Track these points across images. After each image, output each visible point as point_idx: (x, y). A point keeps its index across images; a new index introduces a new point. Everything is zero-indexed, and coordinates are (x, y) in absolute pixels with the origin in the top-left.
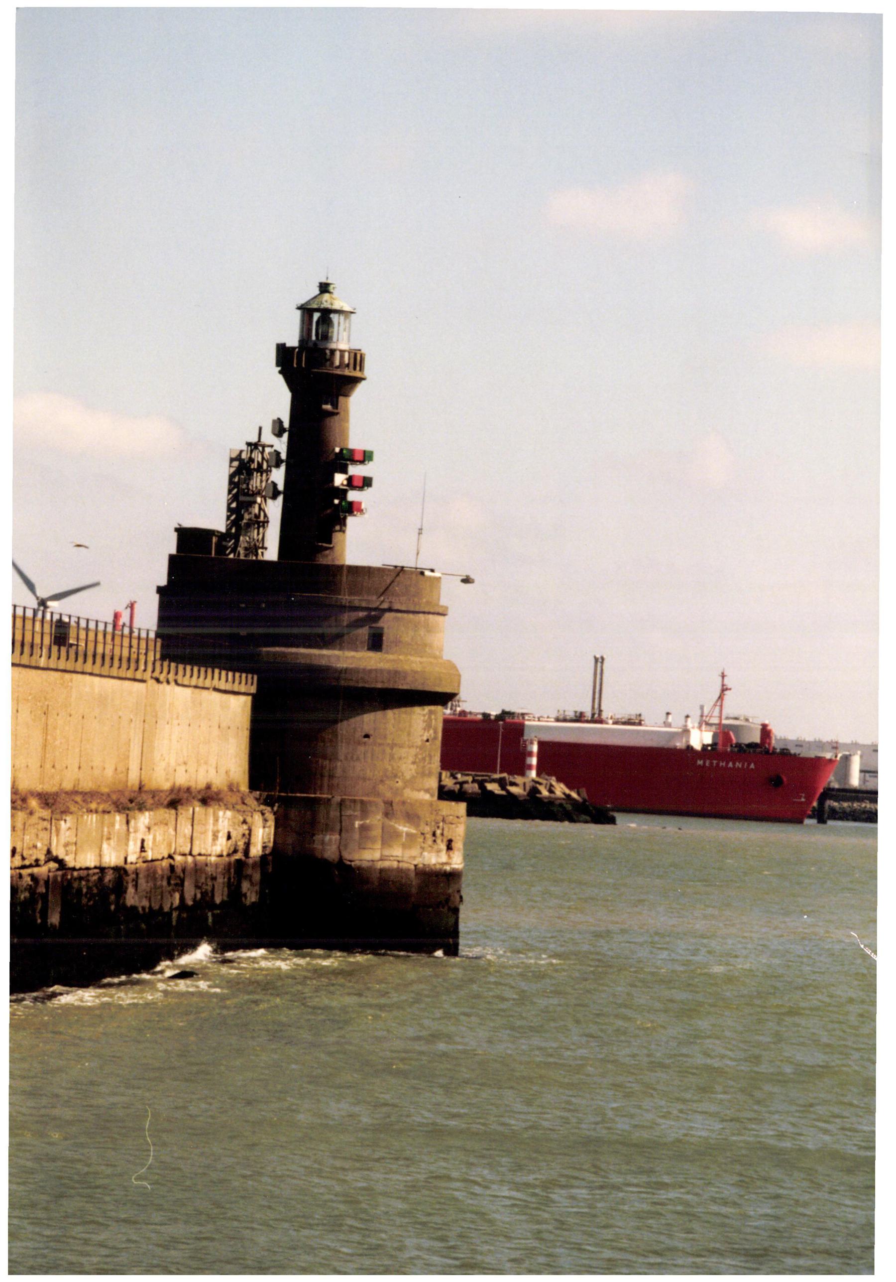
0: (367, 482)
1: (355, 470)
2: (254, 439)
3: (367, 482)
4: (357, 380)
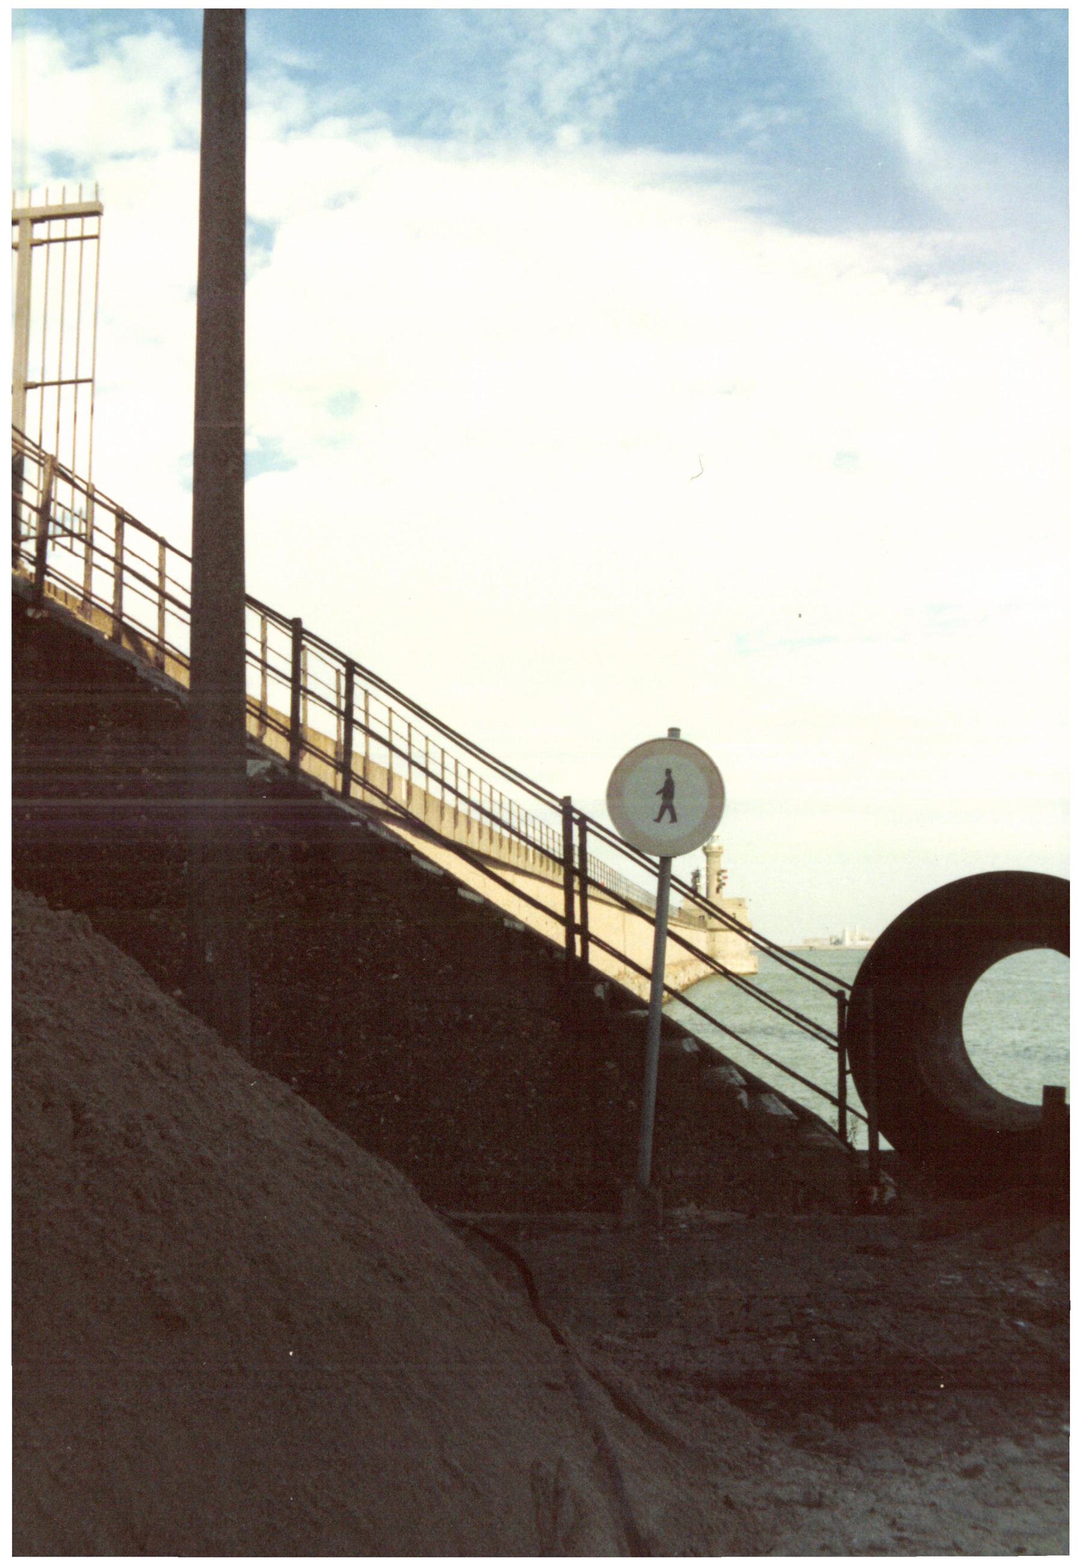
0: (725, 878)
1: (723, 874)
3: (725, 878)
4: (722, 852)
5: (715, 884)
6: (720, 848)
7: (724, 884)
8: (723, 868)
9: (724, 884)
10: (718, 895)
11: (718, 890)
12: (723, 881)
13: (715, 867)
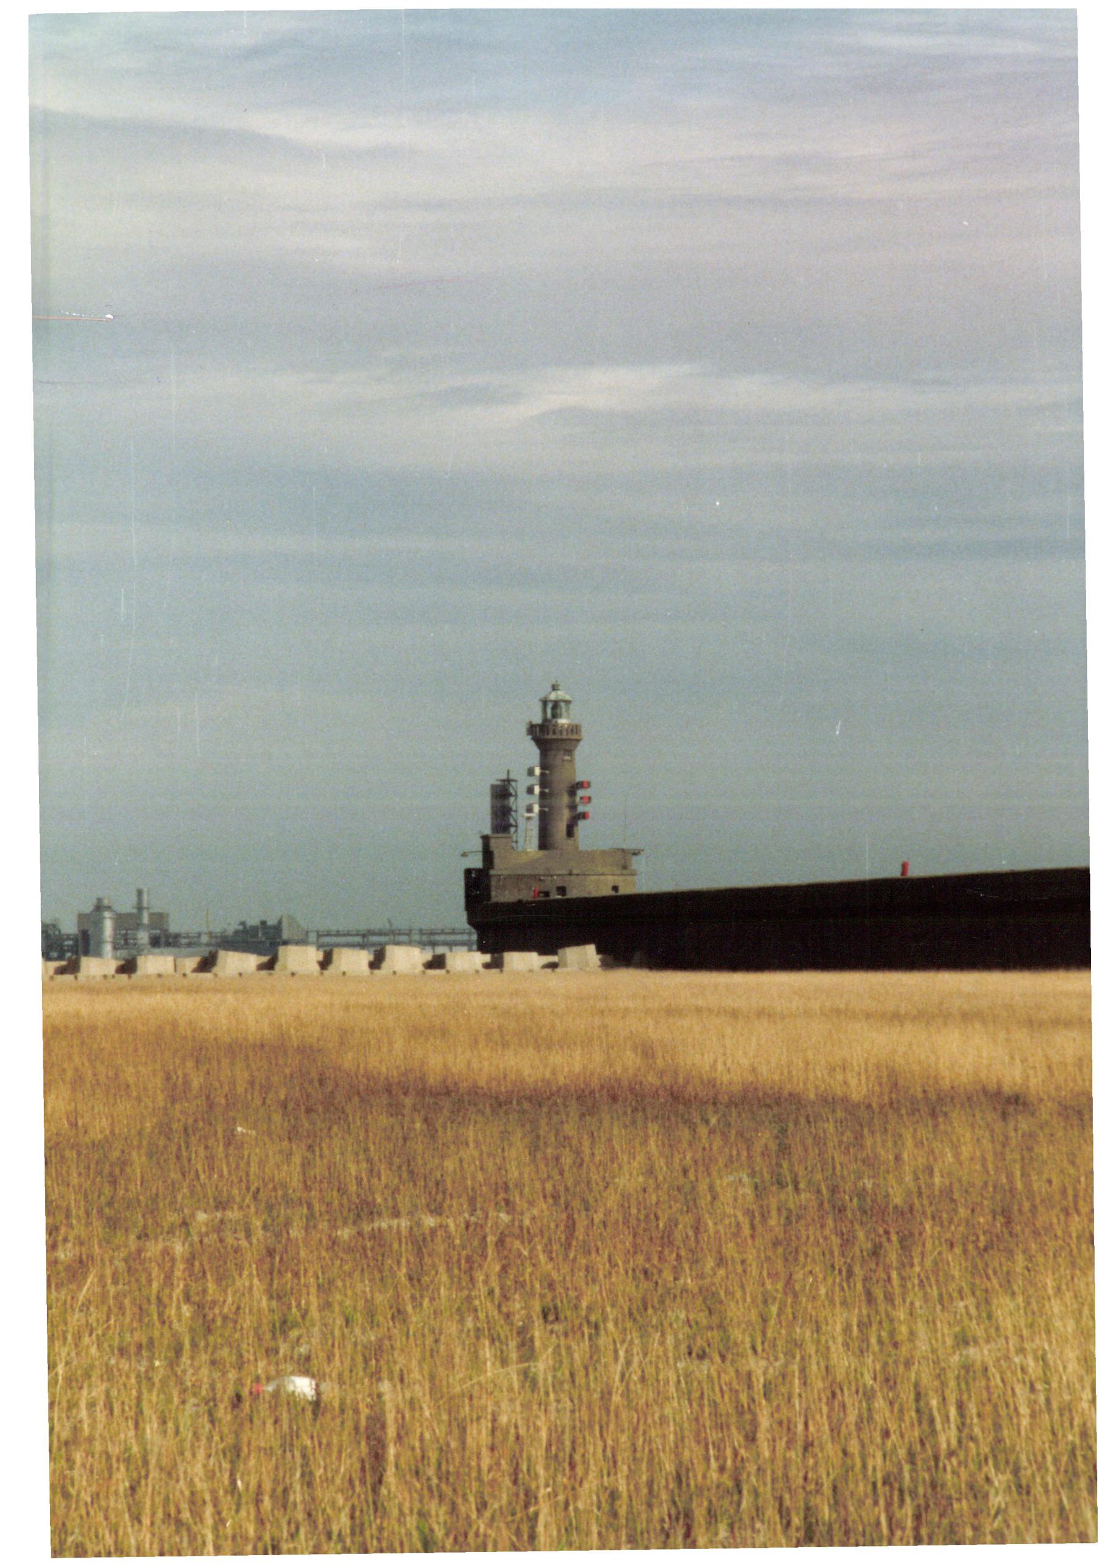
0: (589, 799)
2: (504, 777)
4: (578, 741)
5: (566, 815)
6: (575, 729)
7: (584, 816)
8: (580, 777)
9: (584, 816)
10: (571, 841)
11: (570, 832)
12: (581, 809)
13: (561, 779)
